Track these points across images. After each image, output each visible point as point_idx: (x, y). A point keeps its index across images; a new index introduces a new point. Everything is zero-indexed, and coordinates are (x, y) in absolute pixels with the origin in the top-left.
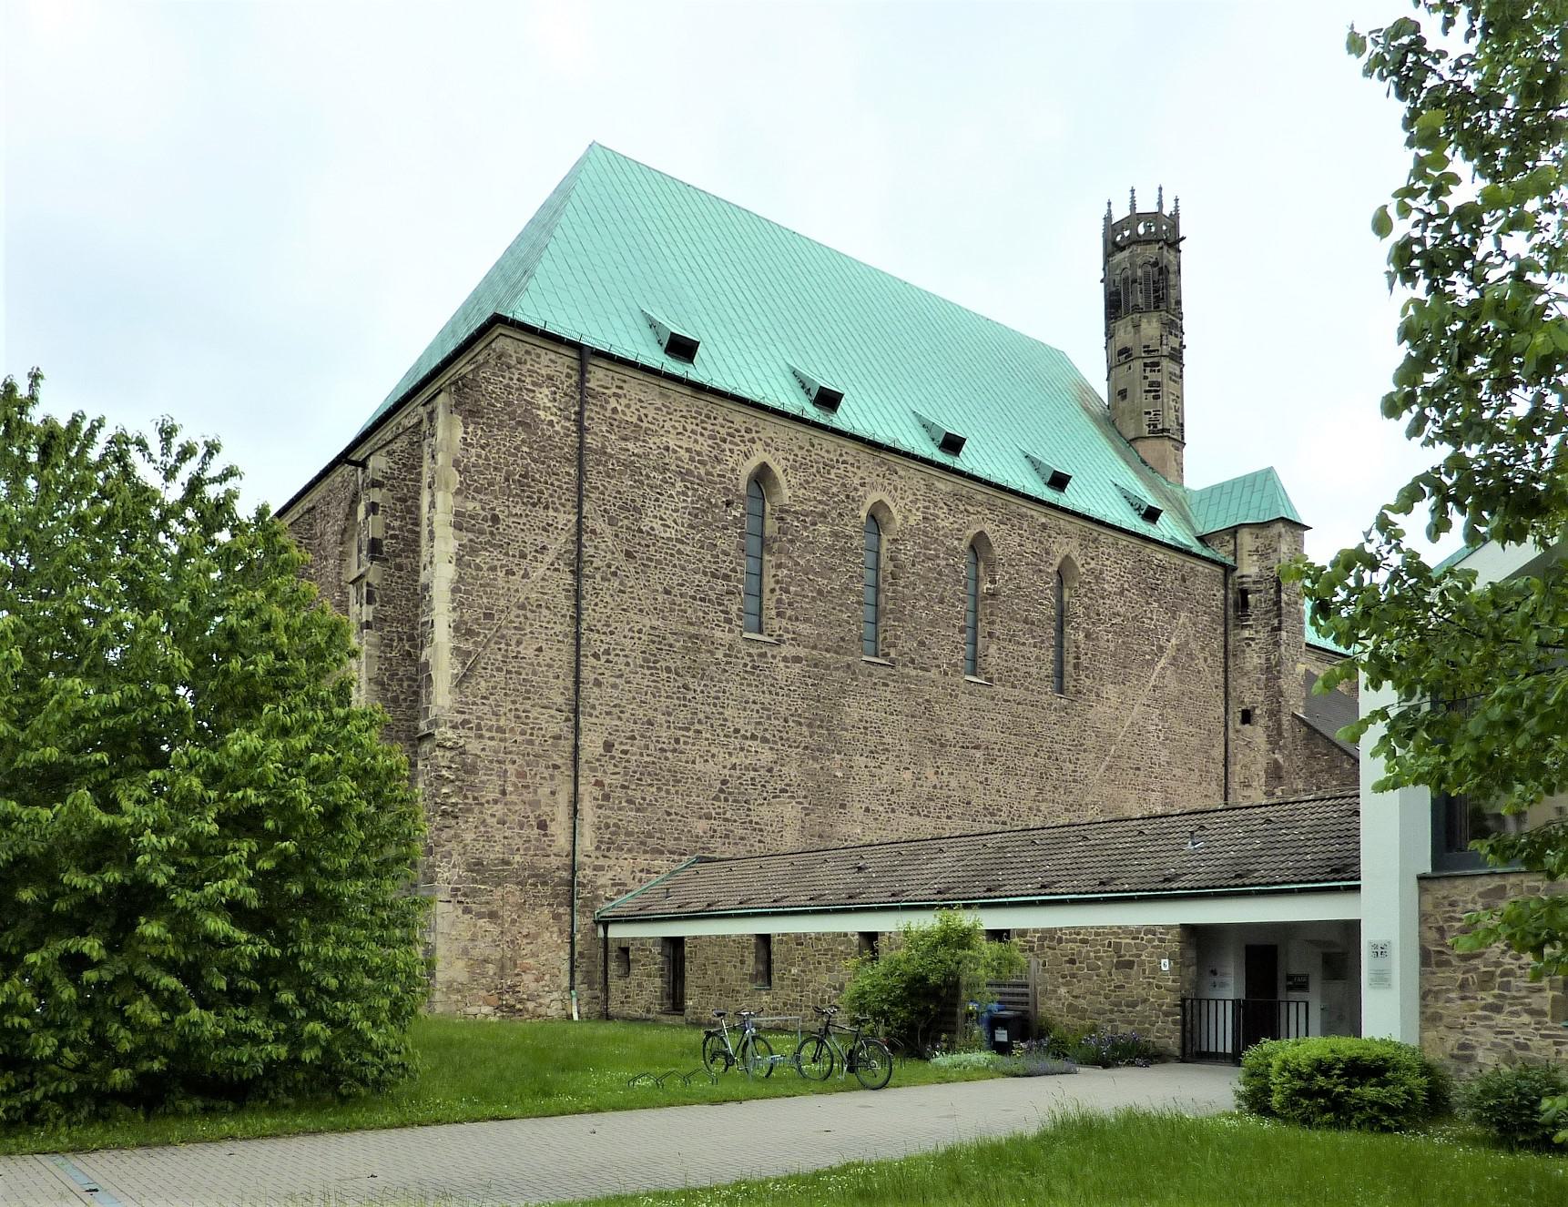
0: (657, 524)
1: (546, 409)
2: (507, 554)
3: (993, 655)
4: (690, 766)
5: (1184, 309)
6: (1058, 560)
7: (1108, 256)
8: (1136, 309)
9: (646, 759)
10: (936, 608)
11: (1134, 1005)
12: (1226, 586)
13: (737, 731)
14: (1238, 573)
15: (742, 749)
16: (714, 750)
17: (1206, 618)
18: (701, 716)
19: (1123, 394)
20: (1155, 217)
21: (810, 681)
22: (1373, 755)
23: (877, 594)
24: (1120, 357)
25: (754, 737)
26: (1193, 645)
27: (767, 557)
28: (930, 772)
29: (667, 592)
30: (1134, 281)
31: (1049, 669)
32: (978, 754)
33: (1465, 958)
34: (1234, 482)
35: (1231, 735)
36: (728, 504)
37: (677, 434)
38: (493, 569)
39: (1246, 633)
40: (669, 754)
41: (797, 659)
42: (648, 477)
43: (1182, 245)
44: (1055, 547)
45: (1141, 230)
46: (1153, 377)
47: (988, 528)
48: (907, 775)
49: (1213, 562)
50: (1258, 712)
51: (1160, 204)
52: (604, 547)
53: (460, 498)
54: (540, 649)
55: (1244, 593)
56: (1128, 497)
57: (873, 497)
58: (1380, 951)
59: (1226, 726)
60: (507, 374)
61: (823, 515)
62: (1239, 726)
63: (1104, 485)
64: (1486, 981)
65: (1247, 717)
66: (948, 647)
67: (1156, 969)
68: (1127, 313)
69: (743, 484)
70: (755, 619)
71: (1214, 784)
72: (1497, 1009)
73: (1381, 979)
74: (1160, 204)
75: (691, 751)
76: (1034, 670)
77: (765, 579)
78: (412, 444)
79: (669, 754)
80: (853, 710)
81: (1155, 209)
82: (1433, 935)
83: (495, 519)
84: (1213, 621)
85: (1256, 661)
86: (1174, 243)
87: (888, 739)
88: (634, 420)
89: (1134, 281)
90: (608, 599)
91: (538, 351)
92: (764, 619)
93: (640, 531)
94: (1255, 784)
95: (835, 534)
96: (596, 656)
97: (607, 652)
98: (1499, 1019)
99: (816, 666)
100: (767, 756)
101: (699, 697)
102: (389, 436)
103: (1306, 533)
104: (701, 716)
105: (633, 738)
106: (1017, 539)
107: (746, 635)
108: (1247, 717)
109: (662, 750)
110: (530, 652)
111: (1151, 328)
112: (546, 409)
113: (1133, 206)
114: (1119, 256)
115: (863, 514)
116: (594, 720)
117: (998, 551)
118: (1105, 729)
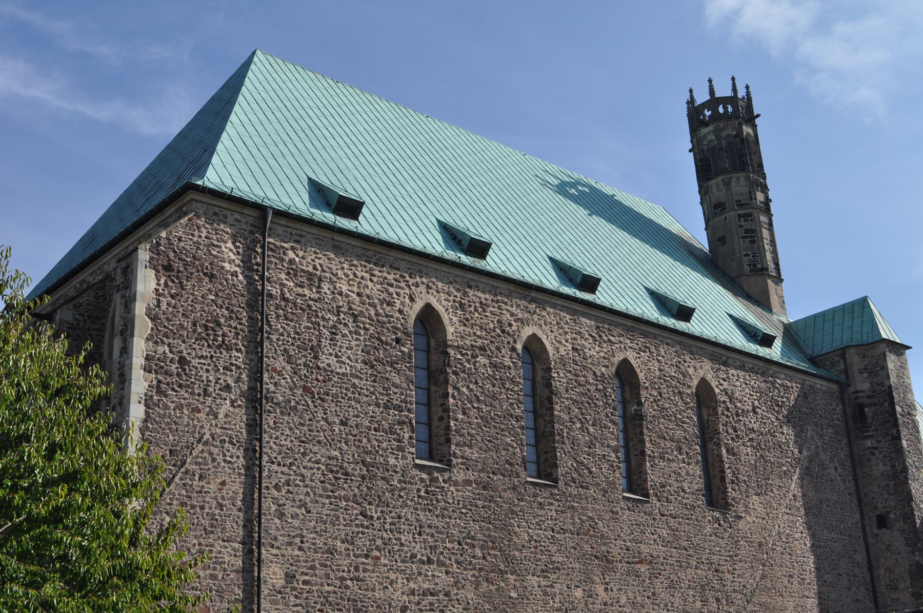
0: (333, 361)
1: (231, 262)
2: (192, 393)
3: (653, 476)
4: (370, 594)
5: (766, 170)
6: (695, 382)
7: (694, 130)
8: (724, 171)
9: (327, 588)
10: (591, 429)
12: (843, 403)
13: (413, 556)
14: (851, 389)
15: (420, 574)
16: (393, 576)
17: (830, 430)
18: (379, 542)
19: (723, 240)
20: (732, 100)
21: (480, 503)
23: (535, 420)
24: (714, 210)
25: (429, 561)
26: (822, 456)
27: (433, 388)
28: (600, 589)
29: (343, 423)
30: (721, 149)
31: (698, 483)
32: (643, 568)
34: (834, 310)
35: (871, 541)
36: (398, 341)
37: (349, 280)
38: (180, 407)
39: (869, 443)
40: (349, 583)
41: (468, 482)
42: (323, 318)
43: (757, 121)
44: (691, 371)
45: (721, 110)
46: (747, 225)
47: (631, 356)
48: (579, 593)
49: (829, 380)
50: (892, 516)
51: (734, 89)
52: (280, 383)
53: (151, 343)
54: (223, 483)
55: (861, 407)
56: (741, 325)
57: (527, 331)
59: (864, 531)
60: (196, 233)
61: (483, 349)
62: (875, 531)
63: (716, 312)
65: (882, 522)
66: (609, 468)
69: (411, 321)
70: (425, 447)
71: (862, 588)
74: (734, 89)
75: (372, 579)
76: (686, 485)
77: (434, 409)
78: (97, 297)
79: (349, 583)
81: (729, 93)
83: (182, 361)
84: (837, 433)
85: (882, 467)
86: (751, 119)
87: (558, 558)
88: (310, 269)
89: (721, 149)
90: (287, 432)
91: (225, 212)
92: (434, 446)
93: (318, 368)
94: (901, 586)
95: (494, 366)
96: (277, 487)
97: (288, 483)
99: (484, 488)
100: (444, 580)
101: (377, 524)
102: (72, 293)
103: (907, 351)
104: (379, 542)
105: (313, 568)
106: (656, 364)
107: (418, 461)
108: (882, 522)
109: (343, 579)
110: (213, 487)
111: (739, 185)
112: (231, 262)
114: (704, 131)
115: (519, 347)
116: (274, 551)
117: (641, 376)
118: (756, 538)
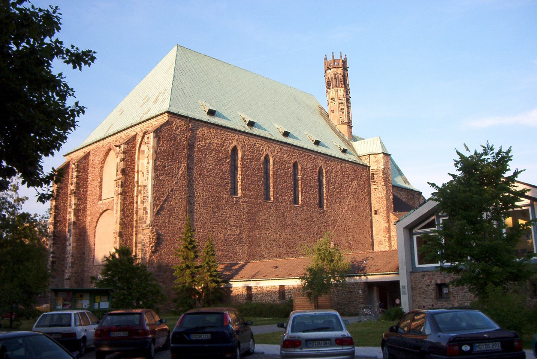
11: (353, 302)
22: (509, 170)
33: (419, 288)
41: (245, 202)
51: (341, 57)
58: (404, 287)
64: (423, 293)
67: (358, 293)
68: (333, 88)
69: (230, 152)
72: (425, 298)
73: (404, 293)
74: (341, 57)
80: (262, 216)
82: (413, 284)
98: (426, 300)
113: (333, 57)
